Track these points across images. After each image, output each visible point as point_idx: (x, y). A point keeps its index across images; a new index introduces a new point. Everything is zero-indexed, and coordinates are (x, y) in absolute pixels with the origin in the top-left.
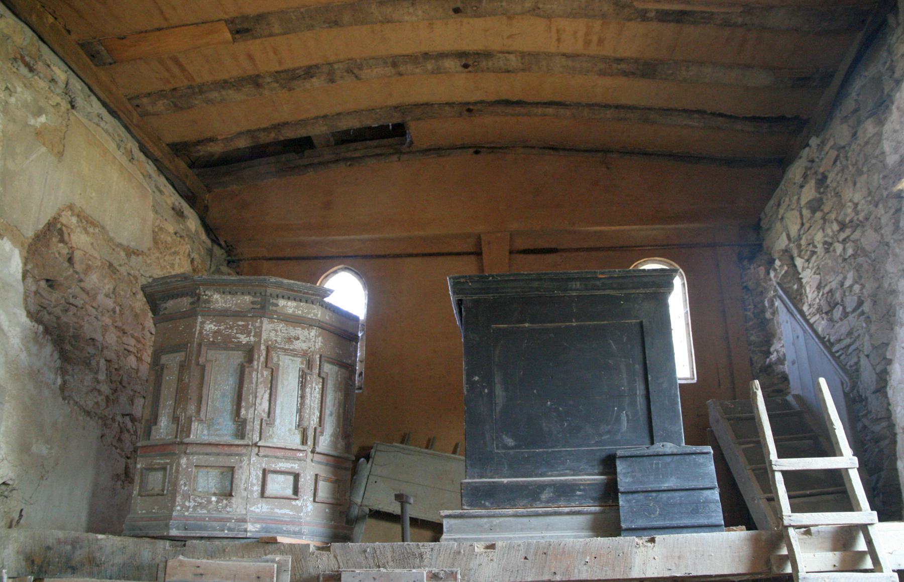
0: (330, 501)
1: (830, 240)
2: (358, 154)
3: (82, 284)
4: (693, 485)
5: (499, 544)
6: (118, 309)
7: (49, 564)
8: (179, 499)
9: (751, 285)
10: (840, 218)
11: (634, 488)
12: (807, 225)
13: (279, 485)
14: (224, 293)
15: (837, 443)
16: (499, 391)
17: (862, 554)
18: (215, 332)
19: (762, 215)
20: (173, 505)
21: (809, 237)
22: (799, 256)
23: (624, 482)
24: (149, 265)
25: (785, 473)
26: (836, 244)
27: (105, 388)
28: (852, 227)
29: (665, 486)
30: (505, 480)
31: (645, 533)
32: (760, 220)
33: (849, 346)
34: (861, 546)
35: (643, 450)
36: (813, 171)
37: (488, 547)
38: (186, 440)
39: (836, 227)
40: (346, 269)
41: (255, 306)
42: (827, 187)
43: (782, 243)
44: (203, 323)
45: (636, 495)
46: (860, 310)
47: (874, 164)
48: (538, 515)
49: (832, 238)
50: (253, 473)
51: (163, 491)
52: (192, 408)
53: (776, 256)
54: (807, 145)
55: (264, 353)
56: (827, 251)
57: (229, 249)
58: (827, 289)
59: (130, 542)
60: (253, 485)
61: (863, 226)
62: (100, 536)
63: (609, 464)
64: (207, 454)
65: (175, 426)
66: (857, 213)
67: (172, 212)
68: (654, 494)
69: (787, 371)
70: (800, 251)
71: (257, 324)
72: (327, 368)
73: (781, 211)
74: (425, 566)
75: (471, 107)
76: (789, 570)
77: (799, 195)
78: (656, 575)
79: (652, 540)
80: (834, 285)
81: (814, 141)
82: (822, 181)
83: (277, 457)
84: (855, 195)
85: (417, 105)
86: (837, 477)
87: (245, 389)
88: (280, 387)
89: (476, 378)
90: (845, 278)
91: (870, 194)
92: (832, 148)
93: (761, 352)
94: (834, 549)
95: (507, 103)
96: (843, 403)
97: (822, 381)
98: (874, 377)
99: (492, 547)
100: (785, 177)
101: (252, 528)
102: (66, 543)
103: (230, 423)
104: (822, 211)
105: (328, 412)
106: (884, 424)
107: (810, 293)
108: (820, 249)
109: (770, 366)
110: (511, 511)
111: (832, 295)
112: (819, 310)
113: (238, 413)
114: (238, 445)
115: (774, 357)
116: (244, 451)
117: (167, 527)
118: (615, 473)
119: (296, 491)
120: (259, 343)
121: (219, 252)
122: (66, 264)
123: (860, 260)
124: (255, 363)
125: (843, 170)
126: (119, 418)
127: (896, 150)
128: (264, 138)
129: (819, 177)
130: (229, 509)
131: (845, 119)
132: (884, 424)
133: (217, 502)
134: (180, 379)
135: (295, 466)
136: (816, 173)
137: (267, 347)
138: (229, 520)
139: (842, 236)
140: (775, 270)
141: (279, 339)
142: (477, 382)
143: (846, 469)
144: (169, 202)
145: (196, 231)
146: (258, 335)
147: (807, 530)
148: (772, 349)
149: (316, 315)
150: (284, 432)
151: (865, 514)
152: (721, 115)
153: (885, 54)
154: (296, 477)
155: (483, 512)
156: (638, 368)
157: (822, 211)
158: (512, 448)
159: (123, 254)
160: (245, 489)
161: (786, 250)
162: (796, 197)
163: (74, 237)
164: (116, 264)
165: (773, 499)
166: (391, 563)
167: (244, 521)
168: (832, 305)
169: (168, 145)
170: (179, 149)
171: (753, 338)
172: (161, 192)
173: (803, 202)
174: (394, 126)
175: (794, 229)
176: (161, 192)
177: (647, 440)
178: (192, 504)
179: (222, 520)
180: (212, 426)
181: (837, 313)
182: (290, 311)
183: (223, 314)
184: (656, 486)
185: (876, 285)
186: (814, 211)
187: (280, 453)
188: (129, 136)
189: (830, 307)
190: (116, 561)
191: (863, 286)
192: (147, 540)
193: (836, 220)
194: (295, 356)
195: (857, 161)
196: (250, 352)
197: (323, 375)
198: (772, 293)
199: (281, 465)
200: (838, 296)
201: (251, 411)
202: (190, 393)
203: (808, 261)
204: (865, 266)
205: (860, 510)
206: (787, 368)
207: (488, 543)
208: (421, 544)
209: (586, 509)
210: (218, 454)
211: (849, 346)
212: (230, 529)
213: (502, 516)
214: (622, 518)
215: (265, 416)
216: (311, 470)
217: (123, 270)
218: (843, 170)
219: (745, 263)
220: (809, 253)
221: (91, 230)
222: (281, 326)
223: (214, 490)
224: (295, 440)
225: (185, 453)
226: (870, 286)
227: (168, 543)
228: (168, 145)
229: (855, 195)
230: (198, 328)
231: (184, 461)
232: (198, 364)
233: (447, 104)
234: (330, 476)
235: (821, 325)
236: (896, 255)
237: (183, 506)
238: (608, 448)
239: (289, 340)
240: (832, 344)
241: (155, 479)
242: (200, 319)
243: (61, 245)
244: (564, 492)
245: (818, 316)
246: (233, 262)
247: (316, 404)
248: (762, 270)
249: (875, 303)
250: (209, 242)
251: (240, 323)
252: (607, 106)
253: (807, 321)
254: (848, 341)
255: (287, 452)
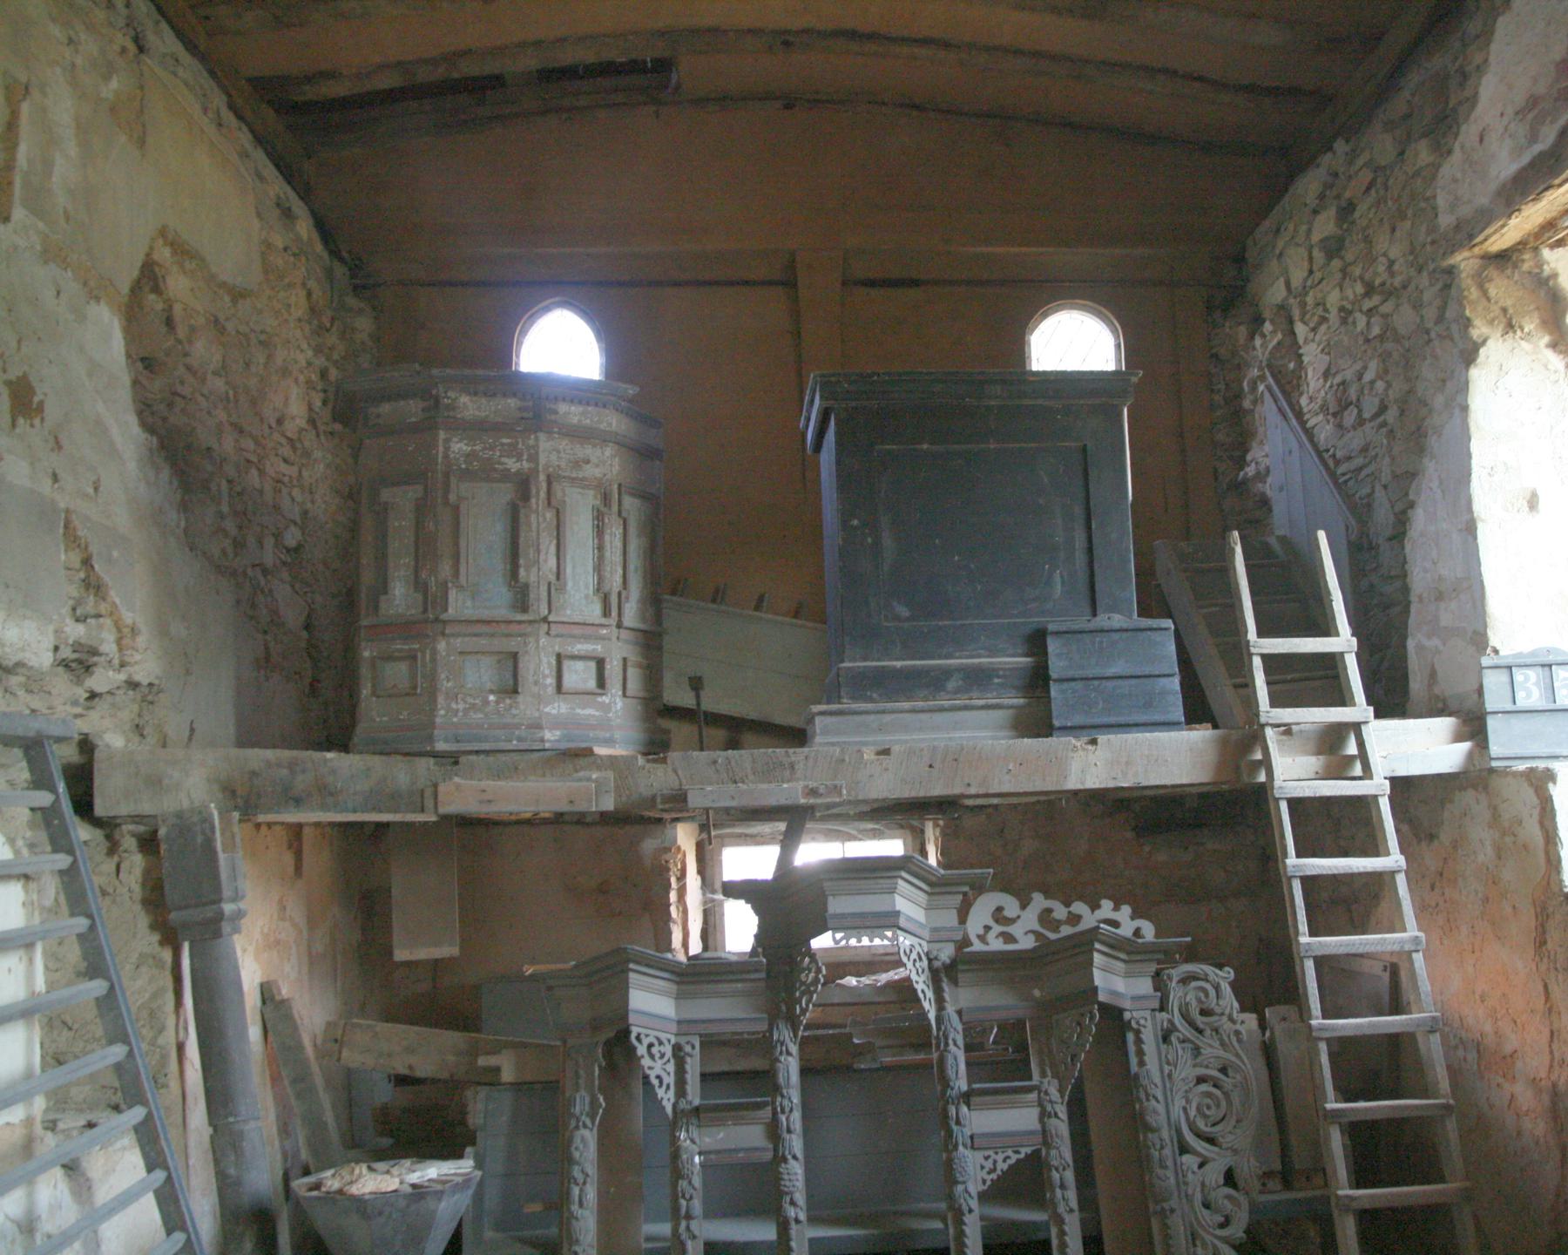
0: (641, 694)
1: (1349, 307)
2: (583, 102)
3: (188, 360)
4: (1147, 670)
5: (896, 749)
6: (231, 393)
7: (259, 795)
8: (441, 700)
9: (1222, 351)
10: (1367, 277)
11: (1070, 673)
12: (1318, 275)
13: (579, 675)
14: (476, 394)
15: (1334, 618)
16: (888, 541)
17: (1352, 758)
18: (468, 455)
19: (1250, 242)
20: (433, 710)
21: (1320, 295)
22: (1302, 320)
23: (1056, 667)
24: (260, 312)
25: (1266, 658)
26: (1358, 315)
27: (230, 525)
28: (1381, 293)
29: (1111, 671)
30: (899, 664)
31: (1085, 732)
32: (1244, 249)
33: (1361, 469)
34: (1352, 749)
35: (1082, 623)
36: (1335, 192)
37: (879, 753)
38: (444, 617)
39: (1360, 289)
40: (565, 304)
41: (525, 415)
42: (1353, 222)
43: (1276, 293)
44: (447, 441)
45: (1073, 684)
46: (1381, 419)
47: (1423, 210)
48: (942, 710)
49: (1353, 303)
50: (545, 660)
51: (415, 688)
52: (445, 569)
53: (1267, 314)
54: (1330, 149)
55: (544, 485)
56: (1344, 321)
57: (354, 270)
58: (1338, 379)
59: (376, 761)
60: (545, 677)
61: (1398, 297)
62: (329, 755)
63: (1037, 642)
64: (476, 635)
65: (420, 597)
66: (1392, 274)
67: (278, 211)
68: (1096, 683)
69: (1268, 492)
70: (1303, 314)
71: (531, 442)
72: (628, 501)
73: (1280, 244)
74: (798, 780)
75: (791, 39)
76: (1262, 778)
77: (1310, 223)
78: (1097, 786)
79: (1094, 742)
80: (1349, 375)
81: (1340, 146)
82: (1346, 212)
83: (573, 636)
84: (1392, 248)
85: (694, 31)
86: (1331, 663)
87: (522, 540)
88: (568, 533)
89: (855, 522)
90: (1365, 368)
91: (1412, 253)
92: (1365, 165)
93: (1231, 458)
94: (1319, 753)
95: (852, 35)
96: (1344, 548)
97: (1322, 535)
98: (1392, 518)
99: (886, 752)
100: (1291, 191)
101: (551, 736)
102: (279, 765)
103: (504, 590)
104: (1342, 258)
105: (631, 567)
106: (1398, 584)
107: (1313, 381)
108: (1333, 316)
109: (1244, 482)
110: (906, 705)
111: (1345, 391)
112: (1324, 408)
113: (514, 573)
114: (520, 622)
115: (1250, 470)
116: (529, 629)
117: (430, 739)
118: (1046, 654)
119: (601, 682)
120: (535, 471)
121: (340, 271)
122: (164, 329)
123: (1389, 346)
124: (533, 500)
125: (1379, 203)
126: (250, 572)
127: (1453, 207)
128: (424, 75)
129: (1344, 204)
130: (514, 711)
131: (1390, 126)
132: (1398, 584)
133: (497, 702)
134: (419, 526)
135: (597, 648)
136: (1338, 197)
137: (549, 477)
138: (517, 726)
139: (1367, 304)
140: (1263, 336)
141: (563, 464)
142: (856, 528)
143: (1342, 654)
144: (272, 193)
145: (310, 239)
146: (534, 458)
147: (1287, 730)
148: (1249, 458)
149: (610, 425)
150: (580, 601)
151: (1360, 710)
152: (1200, 79)
153: (1457, 44)
154: (601, 664)
155: (870, 706)
156: (1078, 510)
157: (1342, 258)
158: (908, 619)
159: (227, 299)
160: (536, 683)
161: (1282, 308)
162: (1304, 227)
163: (171, 281)
164: (222, 318)
165: (1248, 685)
166: (751, 777)
167: (540, 727)
168: (1344, 405)
169: (249, 80)
170: (260, 85)
171: (1220, 437)
172: (262, 179)
173: (1316, 237)
174: (656, 61)
175: (1298, 276)
176: (262, 179)
177: (1088, 610)
178: (461, 706)
179: (505, 726)
180: (478, 593)
181: (1350, 417)
182: (575, 420)
183: (480, 427)
184: (1097, 672)
185: (1406, 387)
186: (1330, 256)
187: (577, 631)
188: (214, 85)
189: (1340, 406)
190: (358, 788)
191: (1389, 385)
192: (399, 758)
193: (1361, 278)
194: (587, 487)
195: (1400, 197)
196: (523, 486)
197: (624, 514)
198: (1256, 372)
199: (579, 646)
200: (1353, 393)
201: (535, 570)
202: (434, 544)
203: (1314, 330)
204: (1395, 355)
205: (1354, 705)
206: (1269, 488)
207: (880, 748)
208: (791, 751)
209: (1006, 701)
210: (493, 635)
211: (1361, 469)
212: (520, 739)
213: (893, 712)
214: (1055, 713)
215: (552, 578)
216: (619, 651)
217: (230, 326)
218: (1379, 203)
219: (1217, 314)
220: (1316, 318)
221: (187, 265)
222: (564, 444)
223: (489, 685)
224: (594, 611)
225: (443, 634)
226: (1398, 387)
227: (432, 761)
228: (249, 80)
229: (1392, 248)
230: (441, 449)
231: (442, 646)
232: (446, 502)
233: (750, 31)
234: (640, 659)
235: (1325, 432)
236: (1435, 357)
237: (448, 709)
238: (1036, 621)
239: (577, 464)
240: (1338, 463)
241: (397, 673)
242: (442, 435)
243: (152, 297)
244: (978, 679)
245: (1321, 417)
246: (364, 287)
247: (618, 558)
248: (1243, 331)
249: (1402, 412)
250: (325, 255)
251: (505, 441)
252: (1018, 52)
253: (1303, 423)
254: (1359, 461)
255: (585, 629)
